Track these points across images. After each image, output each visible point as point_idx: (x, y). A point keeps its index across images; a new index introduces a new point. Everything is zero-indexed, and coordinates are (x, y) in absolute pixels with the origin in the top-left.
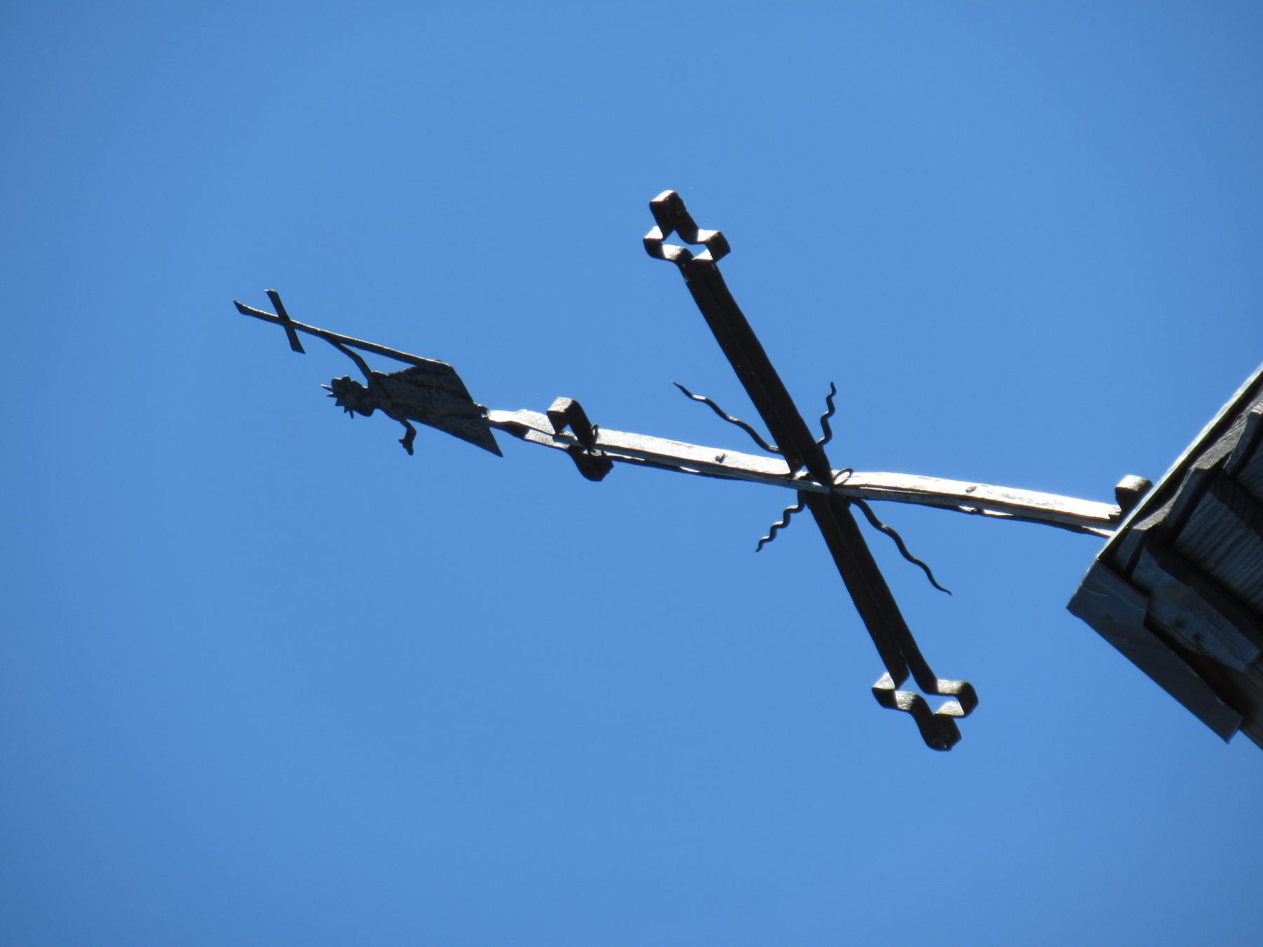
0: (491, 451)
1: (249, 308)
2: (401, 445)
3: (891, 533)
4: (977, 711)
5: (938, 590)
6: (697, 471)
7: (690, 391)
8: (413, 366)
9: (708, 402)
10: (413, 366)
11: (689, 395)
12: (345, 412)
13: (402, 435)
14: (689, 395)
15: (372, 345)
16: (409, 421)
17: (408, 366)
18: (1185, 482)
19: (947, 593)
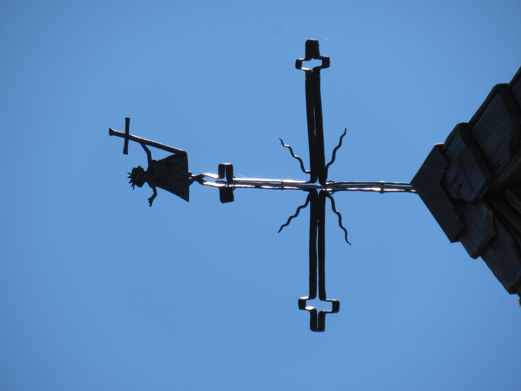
0: (153, 195)
1: (113, 130)
2: (148, 201)
3: (339, 214)
4: (335, 314)
5: (347, 243)
6: (253, 186)
7: (284, 143)
8: (174, 154)
9: (290, 148)
10: (174, 154)
11: (283, 144)
12: (130, 182)
13: (150, 196)
14: (283, 144)
15: (151, 142)
16: (310, 202)
17: (172, 154)
18: (360, 189)
19: (350, 245)
